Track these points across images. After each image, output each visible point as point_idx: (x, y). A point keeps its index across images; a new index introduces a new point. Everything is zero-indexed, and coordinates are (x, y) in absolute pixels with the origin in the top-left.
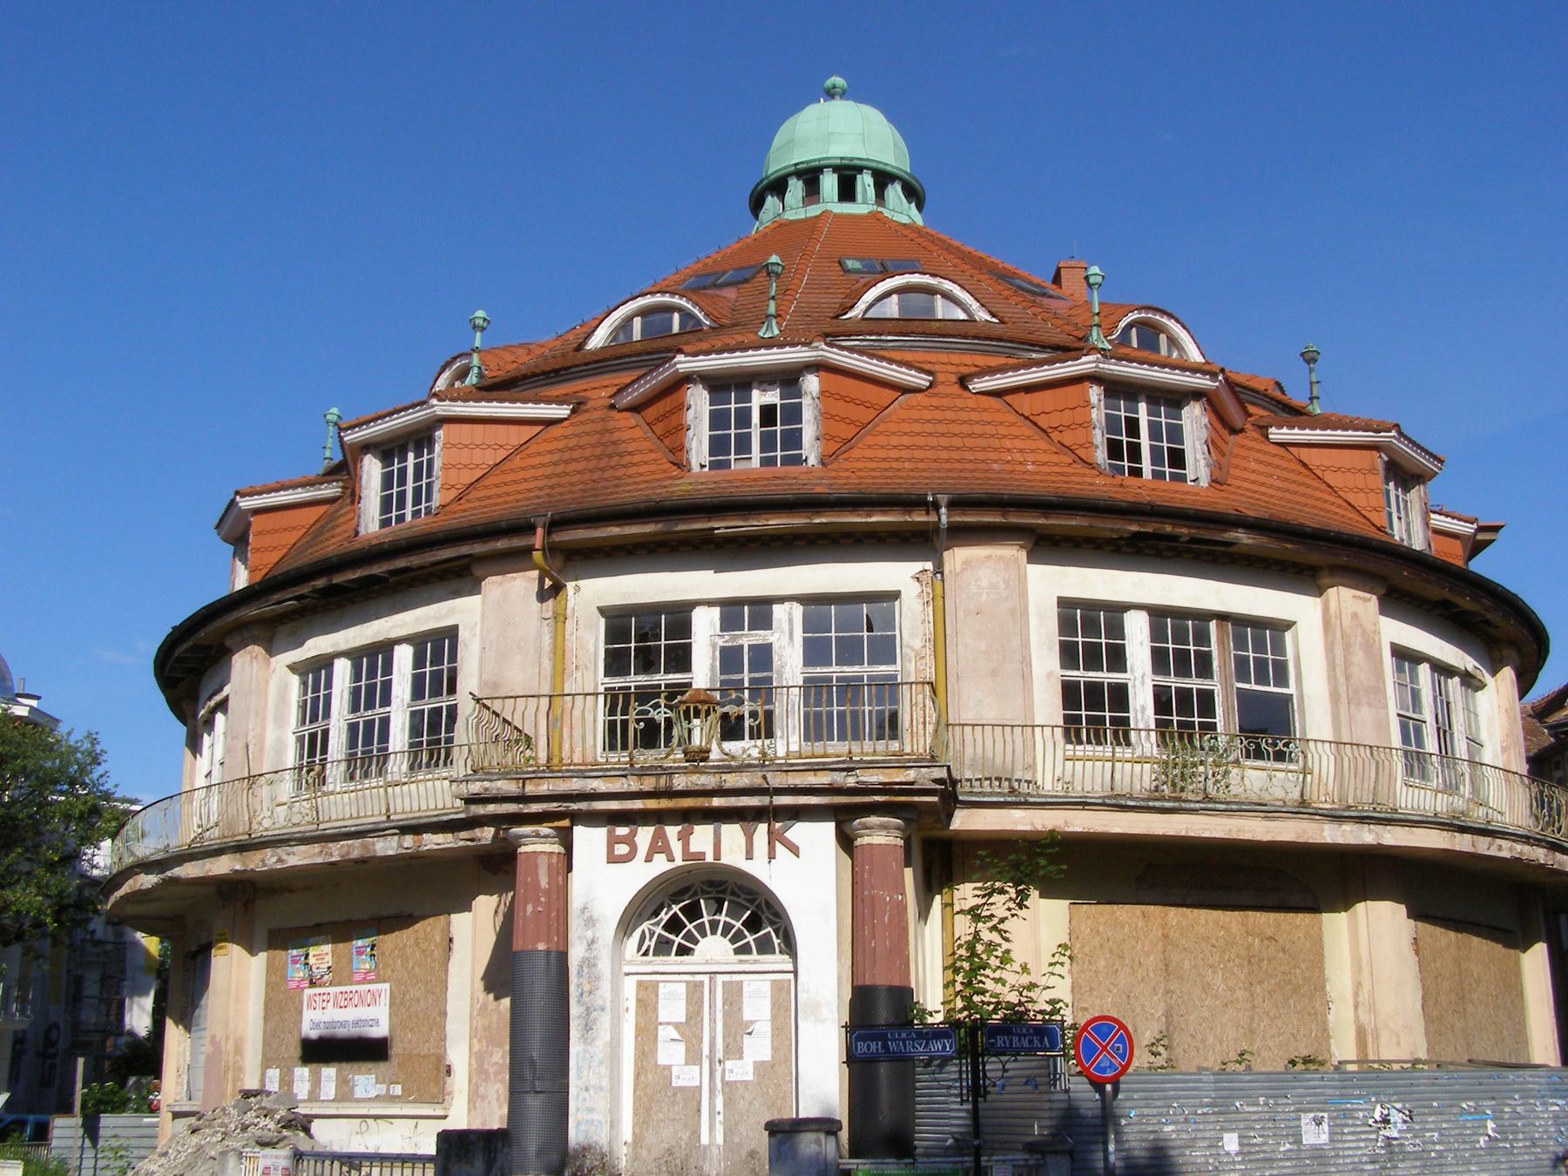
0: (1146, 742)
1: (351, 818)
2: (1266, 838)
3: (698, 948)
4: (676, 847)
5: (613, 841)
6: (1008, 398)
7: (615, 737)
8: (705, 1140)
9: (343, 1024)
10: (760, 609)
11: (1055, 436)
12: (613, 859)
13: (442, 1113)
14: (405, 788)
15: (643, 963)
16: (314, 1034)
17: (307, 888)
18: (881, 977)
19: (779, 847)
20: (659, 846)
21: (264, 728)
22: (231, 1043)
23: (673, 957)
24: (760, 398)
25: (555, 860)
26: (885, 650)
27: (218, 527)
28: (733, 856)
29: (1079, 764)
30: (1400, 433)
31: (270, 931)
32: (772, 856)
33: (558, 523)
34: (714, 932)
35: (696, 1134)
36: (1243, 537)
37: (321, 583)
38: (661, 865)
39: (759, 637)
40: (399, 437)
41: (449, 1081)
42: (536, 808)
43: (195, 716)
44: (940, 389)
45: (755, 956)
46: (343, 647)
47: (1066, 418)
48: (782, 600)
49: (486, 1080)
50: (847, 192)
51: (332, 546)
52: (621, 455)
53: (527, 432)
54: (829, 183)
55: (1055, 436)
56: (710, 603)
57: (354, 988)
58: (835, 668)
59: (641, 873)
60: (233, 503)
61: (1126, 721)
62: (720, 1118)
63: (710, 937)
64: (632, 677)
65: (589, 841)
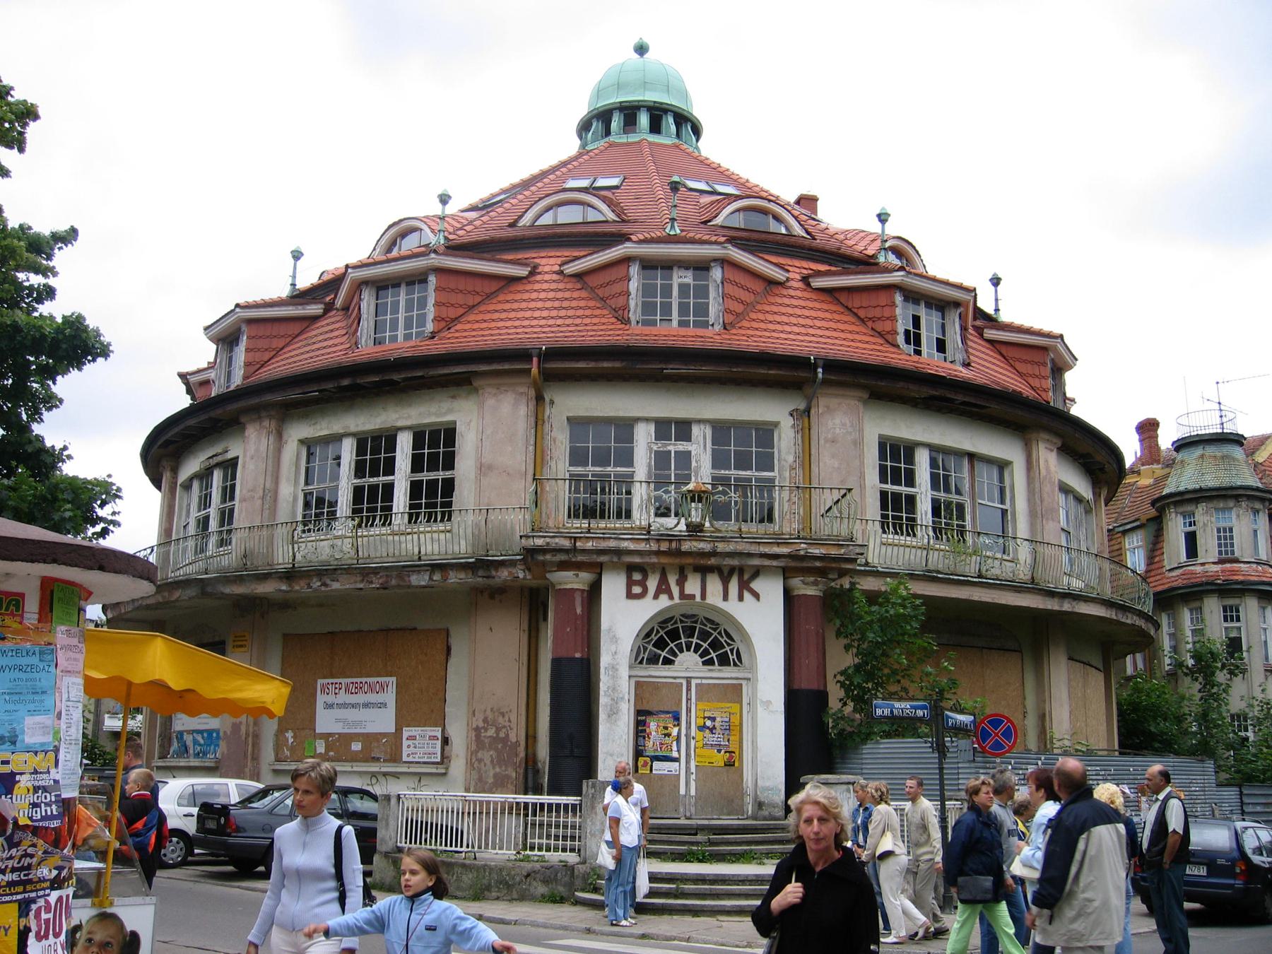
0: (924, 535)
2: (990, 600)
3: (677, 660)
4: (675, 591)
6: (837, 295)
7: (574, 513)
8: (682, 791)
10: (683, 429)
12: (630, 595)
14: (409, 537)
18: (806, 682)
19: (747, 595)
20: (663, 589)
24: (681, 278)
26: (766, 462)
27: (206, 329)
29: (890, 549)
32: (741, 598)
34: (688, 650)
37: (346, 382)
38: (664, 602)
39: (682, 446)
40: (395, 278)
42: (580, 558)
43: (175, 471)
46: (353, 429)
47: (877, 313)
48: (699, 421)
50: (655, 128)
54: (644, 119)
55: (870, 324)
56: (647, 420)
58: (590, 468)
59: (649, 608)
61: (914, 520)
62: (693, 777)
63: (686, 653)
64: (590, 468)
65: (613, 586)
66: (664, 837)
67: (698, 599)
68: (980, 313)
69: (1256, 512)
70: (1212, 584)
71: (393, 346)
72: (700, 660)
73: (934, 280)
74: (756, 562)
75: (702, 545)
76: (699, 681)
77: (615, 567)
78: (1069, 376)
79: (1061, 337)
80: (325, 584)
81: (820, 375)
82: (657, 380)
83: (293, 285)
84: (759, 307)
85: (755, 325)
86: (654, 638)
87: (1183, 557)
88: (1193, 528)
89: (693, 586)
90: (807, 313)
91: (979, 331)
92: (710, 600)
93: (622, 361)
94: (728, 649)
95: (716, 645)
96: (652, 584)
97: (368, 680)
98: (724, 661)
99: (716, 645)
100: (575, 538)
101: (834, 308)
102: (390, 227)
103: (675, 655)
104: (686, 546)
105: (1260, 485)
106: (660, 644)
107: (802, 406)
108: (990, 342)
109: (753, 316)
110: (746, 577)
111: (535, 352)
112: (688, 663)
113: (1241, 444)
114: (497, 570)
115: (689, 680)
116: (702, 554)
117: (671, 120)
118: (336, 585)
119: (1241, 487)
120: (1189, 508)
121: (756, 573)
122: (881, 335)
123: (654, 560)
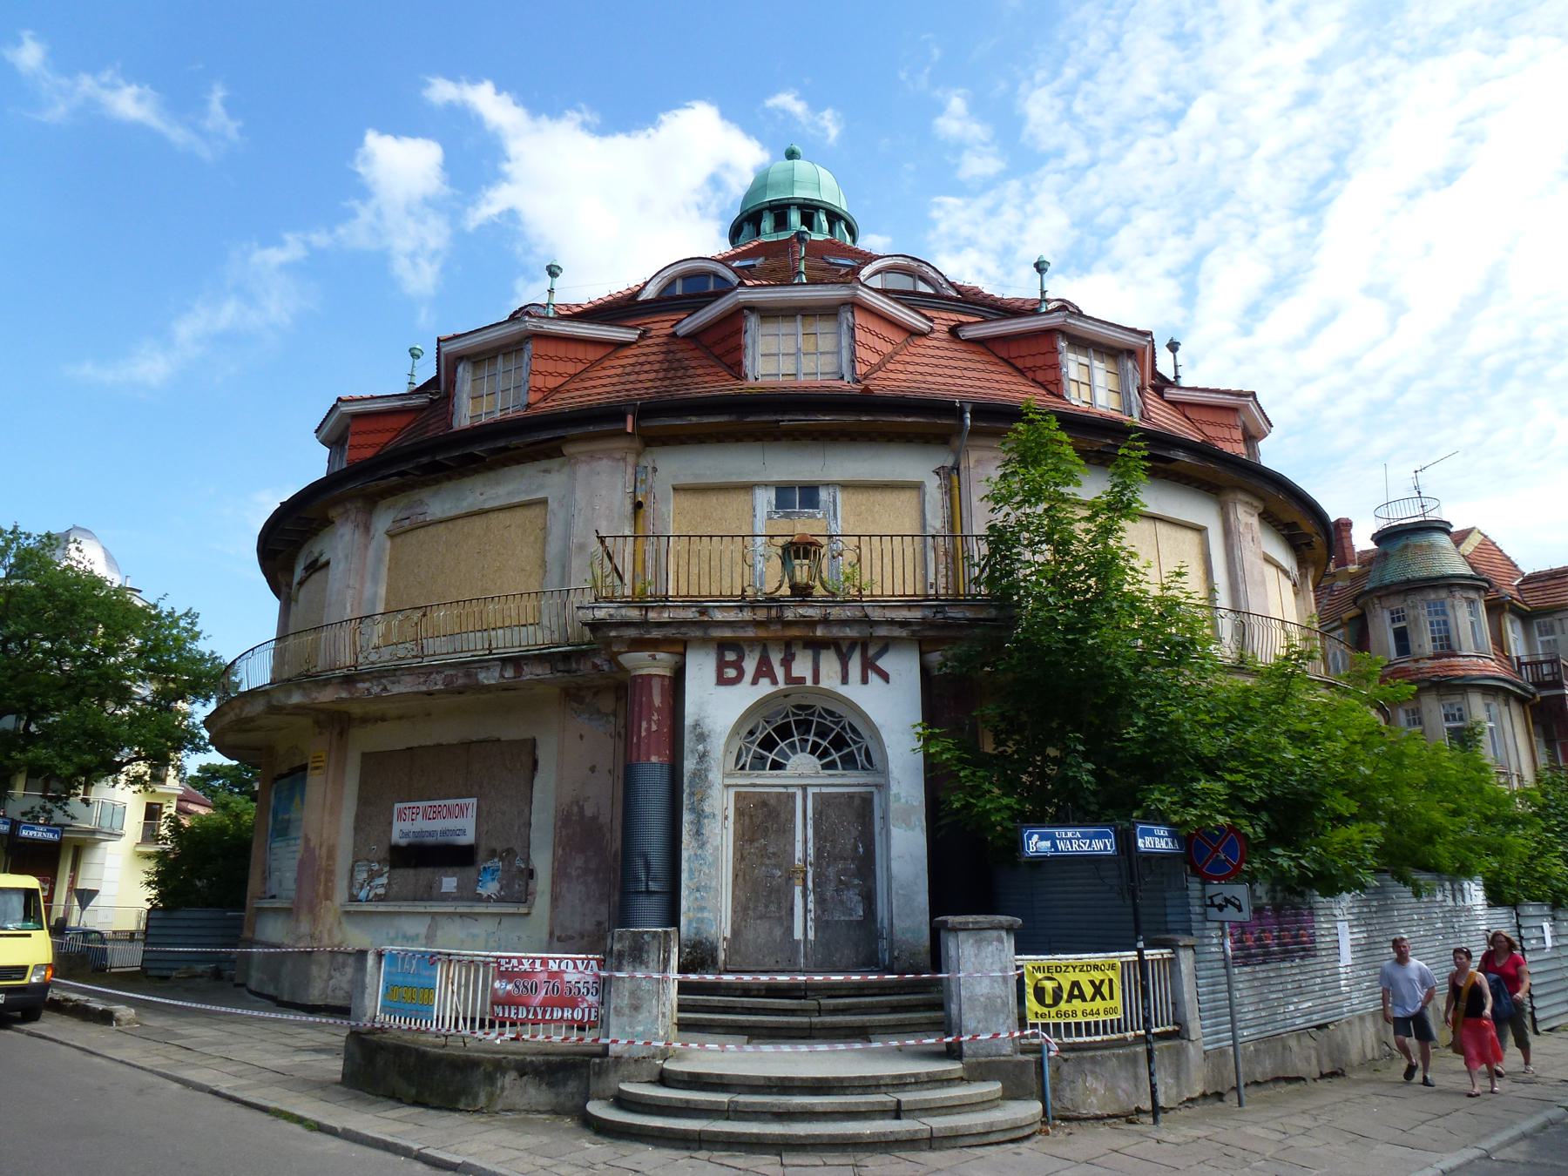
4: (780, 672)
5: (721, 665)
8: (798, 934)
9: (431, 834)
12: (722, 681)
13: (523, 910)
16: (403, 842)
17: (400, 718)
19: (872, 676)
20: (765, 670)
21: (362, 585)
22: (324, 849)
23: (767, 772)
25: (667, 682)
28: (830, 679)
31: (364, 755)
32: (865, 681)
35: (790, 930)
36: (1181, 455)
37: (425, 460)
38: (765, 688)
41: (531, 883)
42: (656, 634)
45: (840, 771)
47: (1039, 361)
48: (827, 484)
50: (807, 220)
51: (434, 431)
52: (685, 369)
53: (593, 354)
54: (795, 218)
57: (442, 803)
65: (700, 670)
67: (809, 683)
69: (1471, 602)
70: (1428, 680)
72: (818, 763)
74: (882, 632)
75: (810, 612)
76: (816, 790)
77: (705, 642)
78: (1262, 445)
79: (1253, 394)
80: (385, 689)
84: (898, 358)
85: (891, 375)
86: (759, 736)
88: (1403, 624)
90: (951, 363)
92: (825, 683)
93: (730, 414)
94: (854, 747)
95: (839, 743)
96: (750, 665)
97: (448, 802)
98: (849, 762)
99: (839, 743)
101: (986, 358)
103: (787, 758)
104: (789, 615)
106: (768, 744)
107: (949, 463)
108: (1172, 403)
109: (889, 366)
110: (871, 652)
112: (802, 767)
113: (1448, 533)
114: (578, 663)
115: (804, 788)
116: (811, 623)
117: (823, 217)
118: (396, 689)
121: (886, 645)
122: (1042, 385)
123: (750, 633)
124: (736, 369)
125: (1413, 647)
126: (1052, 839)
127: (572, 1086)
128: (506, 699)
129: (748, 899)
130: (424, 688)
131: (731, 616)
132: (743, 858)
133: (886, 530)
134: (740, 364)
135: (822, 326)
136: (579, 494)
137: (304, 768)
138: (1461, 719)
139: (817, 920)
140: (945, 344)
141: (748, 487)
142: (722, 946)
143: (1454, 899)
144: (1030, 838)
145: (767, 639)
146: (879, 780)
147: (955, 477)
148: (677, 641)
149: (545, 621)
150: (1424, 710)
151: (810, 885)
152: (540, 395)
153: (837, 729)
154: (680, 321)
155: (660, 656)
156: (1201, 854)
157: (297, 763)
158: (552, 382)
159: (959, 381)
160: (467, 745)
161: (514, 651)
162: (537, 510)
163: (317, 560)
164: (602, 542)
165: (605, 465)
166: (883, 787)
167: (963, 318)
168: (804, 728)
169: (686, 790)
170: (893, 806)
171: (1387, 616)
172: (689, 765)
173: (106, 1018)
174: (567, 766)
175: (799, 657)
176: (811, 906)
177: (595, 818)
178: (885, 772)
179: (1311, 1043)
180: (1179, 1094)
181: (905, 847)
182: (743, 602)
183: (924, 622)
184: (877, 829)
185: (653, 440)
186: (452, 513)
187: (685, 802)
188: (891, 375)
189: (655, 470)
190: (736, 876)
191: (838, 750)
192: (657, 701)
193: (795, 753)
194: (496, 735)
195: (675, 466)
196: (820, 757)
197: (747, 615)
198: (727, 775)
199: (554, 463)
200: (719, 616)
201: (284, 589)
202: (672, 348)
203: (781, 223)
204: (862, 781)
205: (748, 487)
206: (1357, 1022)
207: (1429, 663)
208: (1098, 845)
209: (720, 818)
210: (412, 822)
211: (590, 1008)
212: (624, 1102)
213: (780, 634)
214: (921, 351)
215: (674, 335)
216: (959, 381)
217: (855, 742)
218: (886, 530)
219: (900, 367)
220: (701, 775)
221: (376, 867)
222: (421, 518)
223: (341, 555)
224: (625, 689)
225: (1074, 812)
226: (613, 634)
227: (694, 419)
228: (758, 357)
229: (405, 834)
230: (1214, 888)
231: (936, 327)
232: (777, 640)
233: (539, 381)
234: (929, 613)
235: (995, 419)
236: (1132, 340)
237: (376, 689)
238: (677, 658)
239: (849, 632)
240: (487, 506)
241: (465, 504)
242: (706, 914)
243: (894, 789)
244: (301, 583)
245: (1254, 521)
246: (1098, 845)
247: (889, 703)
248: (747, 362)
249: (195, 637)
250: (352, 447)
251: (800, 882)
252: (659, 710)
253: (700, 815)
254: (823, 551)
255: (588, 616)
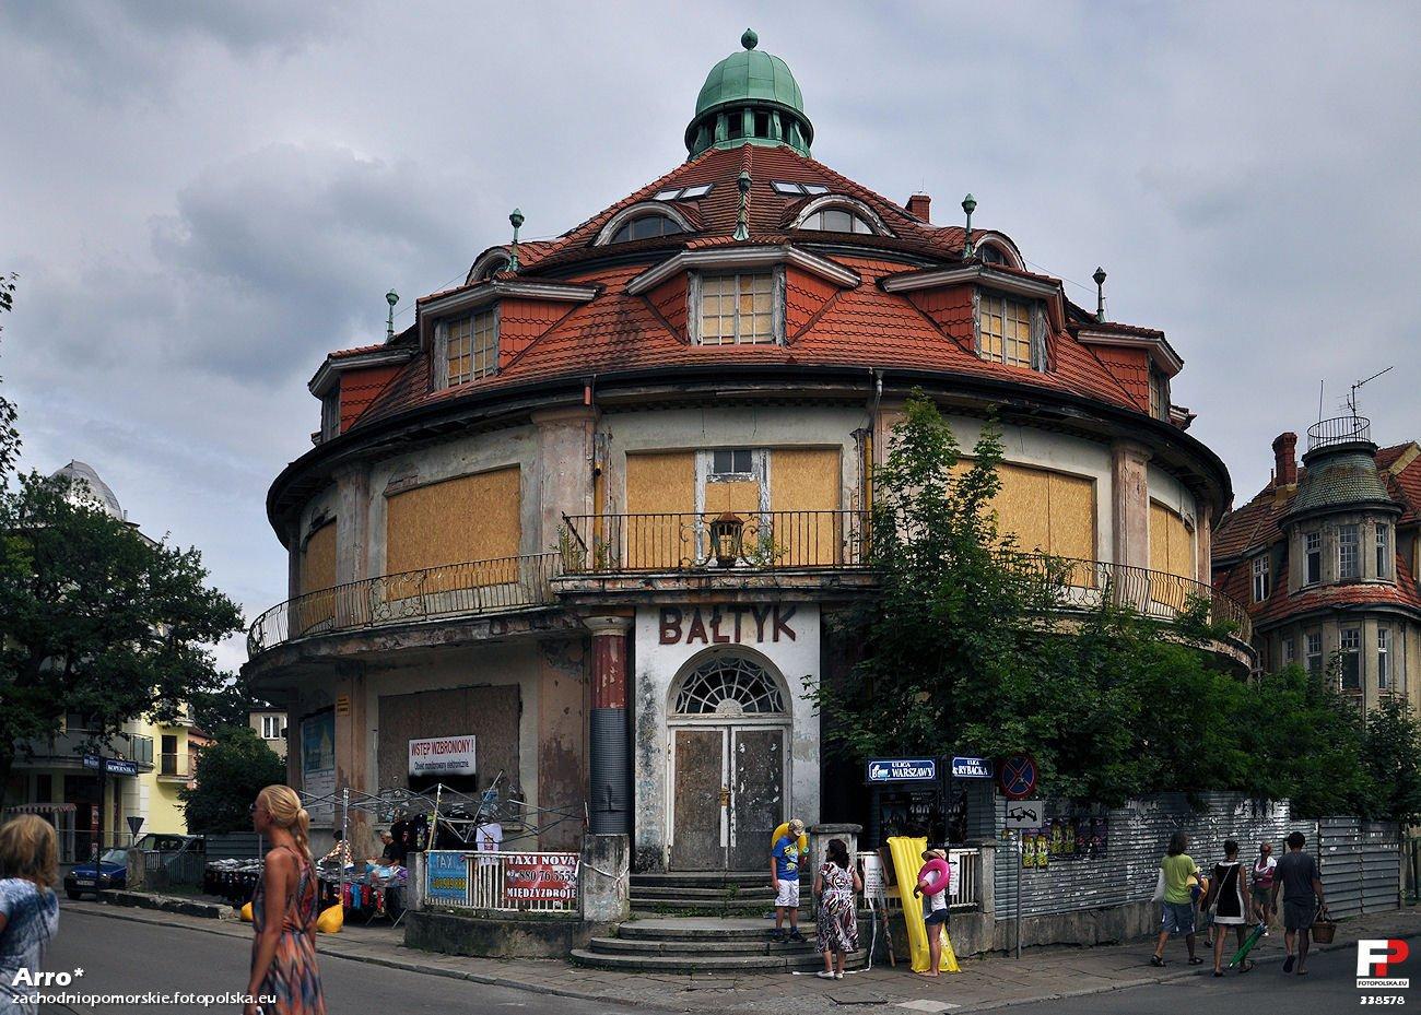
1: (511, 605)
4: (709, 632)
5: (663, 628)
8: (724, 843)
9: (440, 765)
11: (945, 329)
12: (664, 641)
15: (681, 718)
16: (418, 772)
17: (408, 666)
19: (782, 635)
22: (355, 779)
23: (701, 715)
25: (621, 641)
27: (309, 384)
28: (749, 640)
30: (1163, 339)
31: (379, 697)
32: (776, 639)
33: (600, 385)
36: (1074, 414)
37: (414, 428)
38: (698, 646)
42: (611, 602)
44: (864, 288)
48: (759, 449)
49: (1162, 781)
50: (761, 131)
53: (555, 315)
54: (749, 121)
55: (945, 329)
57: (448, 739)
59: (684, 652)
60: (326, 363)
63: (721, 702)
66: (703, 891)
67: (732, 641)
68: (1072, 310)
69: (1381, 528)
70: (1331, 607)
71: (468, 385)
73: (1032, 277)
75: (732, 581)
76: (739, 729)
77: (650, 609)
79: (1161, 334)
80: (397, 643)
81: (880, 389)
82: (714, 406)
83: (391, 331)
87: (1306, 581)
88: (1316, 550)
89: (727, 629)
91: (1073, 332)
93: (674, 385)
96: (686, 627)
97: (451, 739)
98: (764, 706)
99: (757, 690)
100: (604, 580)
101: (907, 312)
102: (478, 259)
104: (716, 584)
105: (1388, 498)
106: (702, 691)
107: (864, 426)
108: (1086, 345)
110: (781, 615)
111: (587, 381)
114: (551, 621)
115: (729, 727)
116: (733, 591)
117: (777, 120)
118: (407, 644)
119: (1368, 502)
120: (1314, 527)
121: (793, 609)
122: (956, 341)
123: (685, 600)
124: (681, 333)
125: (1323, 573)
126: (889, 767)
127: (561, 941)
128: (499, 652)
129: (687, 816)
130: (430, 643)
131: (671, 586)
132: (682, 784)
133: (806, 498)
134: (684, 327)
135: (759, 287)
136: (546, 462)
137: (331, 709)
138: (1356, 645)
139: (737, 832)
140: (871, 299)
141: (691, 453)
142: (667, 852)
143: (1254, 813)
144: (873, 767)
145: (699, 604)
146: (787, 721)
147: (869, 441)
148: (630, 606)
149: (523, 580)
150: (1325, 636)
151: (733, 805)
152: (509, 359)
153: (756, 678)
154: (631, 281)
155: (616, 619)
156: (1005, 775)
157: (323, 705)
158: (520, 346)
159: (879, 340)
160: (464, 690)
161: (499, 610)
162: (512, 475)
163: (323, 517)
164: (568, 521)
165: (567, 432)
166: (789, 726)
167: (892, 267)
168: (729, 677)
169: (638, 731)
170: (796, 741)
171: (1305, 541)
172: (640, 710)
173: (213, 913)
174: (546, 712)
175: (724, 620)
176: (733, 821)
177: (569, 752)
178: (790, 715)
179: (1091, 920)
180: (972, 948)
181: (804, 774)
182: (679, 572)
183: (822, 589)
184: (785, 760)
185: (608, 410)
186: (440, 477)
187: (637, 740)
188: (819, 337)
189: (611, 437)
190: (677, 799)
191: (756, 696)
192: (614, 658)
193: (722, 698)
194: (487, 682)
195: (631, 434)
196: (742, 702)
197: (682, 585)
198: (670, 718)
199: (524, 431)
200: (660, 586)
201: (291, 540)
202: (626, 307)
203: (735, 129)
204: (774, 721)
205: (691, 453)
206: (1137, 906)
207: (1335, 590)
208: (922, 772)
209: (664, 752)
210: (423, 756)
211: (571, 889)
212: (594, 948)
213: (709, 600)
214: (848, 307)
215: (625, 293)
216: (879, 340)
217: (770, 689)
218: (806, 498)
219: (827, 327)
220: (648, 718)
221: (398, 793)
222: (413, 481)
223: (346, 515)
224: (587, 643)
225: (914, 749)
226: (578, 602)
227: (643, 390)
228: (701, 321)
229: (420, 766)
230: (1012, 805)
231: (864, 279)
232: (707, 605)
233: (508, 345)
234: (826, 581)
235: (902, 381)
236: (1041, 289)
237: (390, 644)
238: (629, 621)
239: (763, 598)
240: (469, 471)
241: (450, 469)
242: (654, 827)
243: (796, 728)
244: (309, 537)
245: (1142, 470)
246: (922, 772)
247: (794, 655)
248: (691, 326)
249: (202, 574)
250: (345, 404)
251: (724, 802)
252: (616, 665)
253: (648, 750)
254: (743, 528)
255: (557, 587)
